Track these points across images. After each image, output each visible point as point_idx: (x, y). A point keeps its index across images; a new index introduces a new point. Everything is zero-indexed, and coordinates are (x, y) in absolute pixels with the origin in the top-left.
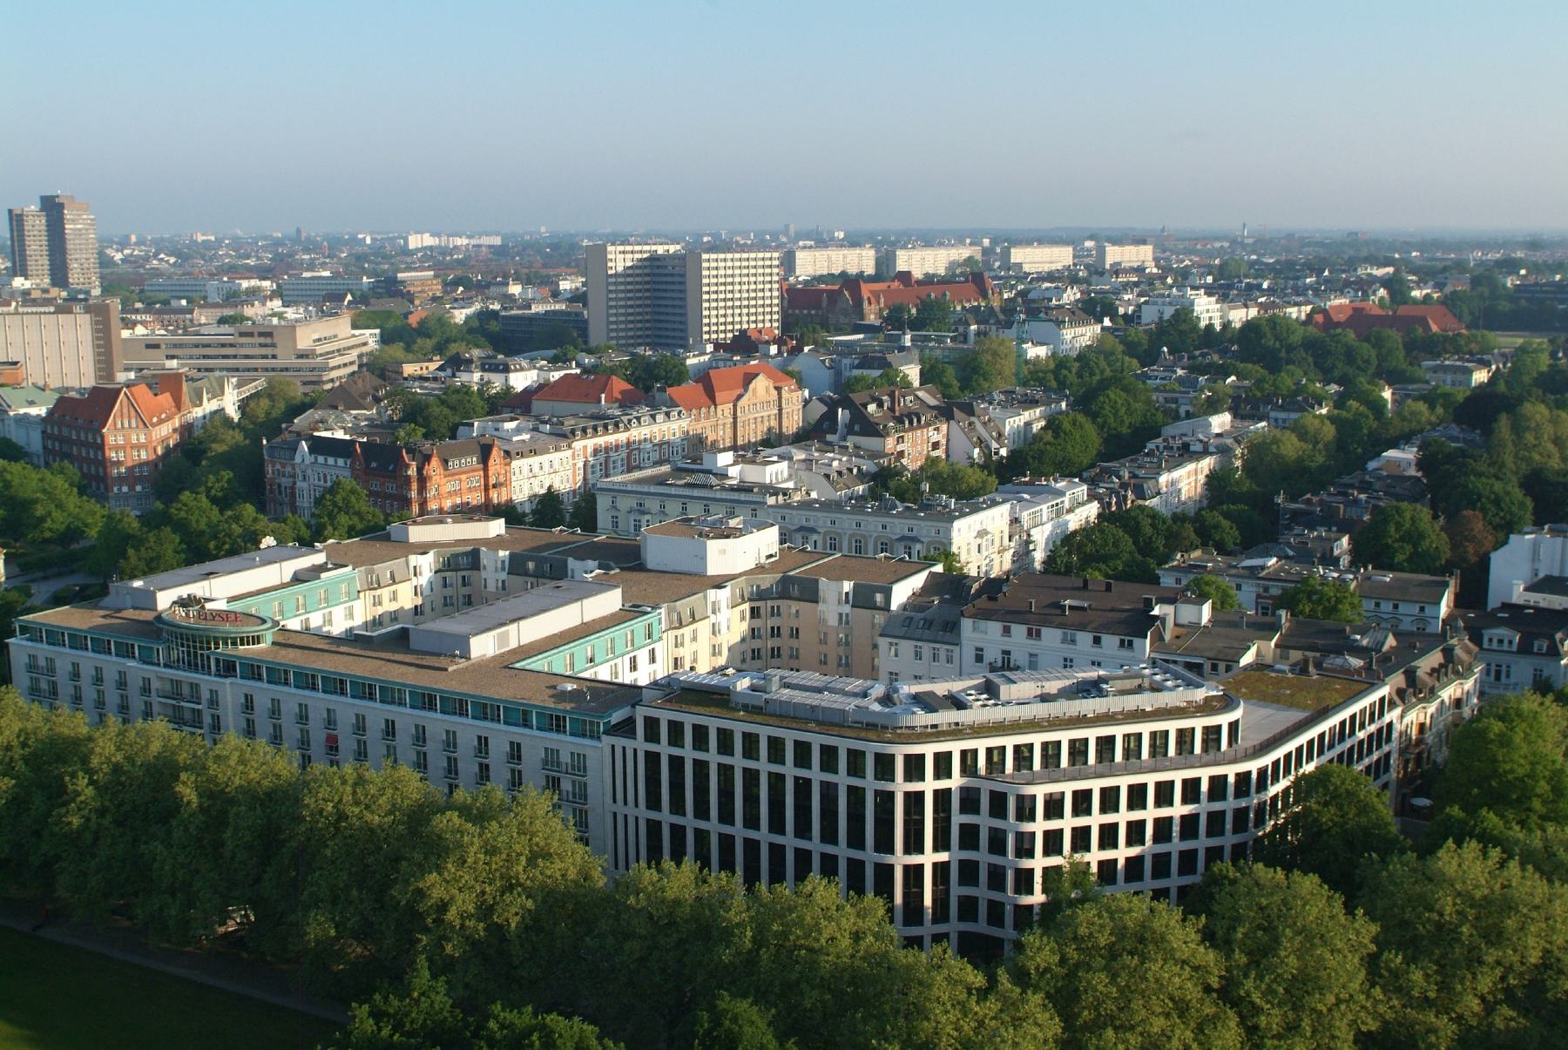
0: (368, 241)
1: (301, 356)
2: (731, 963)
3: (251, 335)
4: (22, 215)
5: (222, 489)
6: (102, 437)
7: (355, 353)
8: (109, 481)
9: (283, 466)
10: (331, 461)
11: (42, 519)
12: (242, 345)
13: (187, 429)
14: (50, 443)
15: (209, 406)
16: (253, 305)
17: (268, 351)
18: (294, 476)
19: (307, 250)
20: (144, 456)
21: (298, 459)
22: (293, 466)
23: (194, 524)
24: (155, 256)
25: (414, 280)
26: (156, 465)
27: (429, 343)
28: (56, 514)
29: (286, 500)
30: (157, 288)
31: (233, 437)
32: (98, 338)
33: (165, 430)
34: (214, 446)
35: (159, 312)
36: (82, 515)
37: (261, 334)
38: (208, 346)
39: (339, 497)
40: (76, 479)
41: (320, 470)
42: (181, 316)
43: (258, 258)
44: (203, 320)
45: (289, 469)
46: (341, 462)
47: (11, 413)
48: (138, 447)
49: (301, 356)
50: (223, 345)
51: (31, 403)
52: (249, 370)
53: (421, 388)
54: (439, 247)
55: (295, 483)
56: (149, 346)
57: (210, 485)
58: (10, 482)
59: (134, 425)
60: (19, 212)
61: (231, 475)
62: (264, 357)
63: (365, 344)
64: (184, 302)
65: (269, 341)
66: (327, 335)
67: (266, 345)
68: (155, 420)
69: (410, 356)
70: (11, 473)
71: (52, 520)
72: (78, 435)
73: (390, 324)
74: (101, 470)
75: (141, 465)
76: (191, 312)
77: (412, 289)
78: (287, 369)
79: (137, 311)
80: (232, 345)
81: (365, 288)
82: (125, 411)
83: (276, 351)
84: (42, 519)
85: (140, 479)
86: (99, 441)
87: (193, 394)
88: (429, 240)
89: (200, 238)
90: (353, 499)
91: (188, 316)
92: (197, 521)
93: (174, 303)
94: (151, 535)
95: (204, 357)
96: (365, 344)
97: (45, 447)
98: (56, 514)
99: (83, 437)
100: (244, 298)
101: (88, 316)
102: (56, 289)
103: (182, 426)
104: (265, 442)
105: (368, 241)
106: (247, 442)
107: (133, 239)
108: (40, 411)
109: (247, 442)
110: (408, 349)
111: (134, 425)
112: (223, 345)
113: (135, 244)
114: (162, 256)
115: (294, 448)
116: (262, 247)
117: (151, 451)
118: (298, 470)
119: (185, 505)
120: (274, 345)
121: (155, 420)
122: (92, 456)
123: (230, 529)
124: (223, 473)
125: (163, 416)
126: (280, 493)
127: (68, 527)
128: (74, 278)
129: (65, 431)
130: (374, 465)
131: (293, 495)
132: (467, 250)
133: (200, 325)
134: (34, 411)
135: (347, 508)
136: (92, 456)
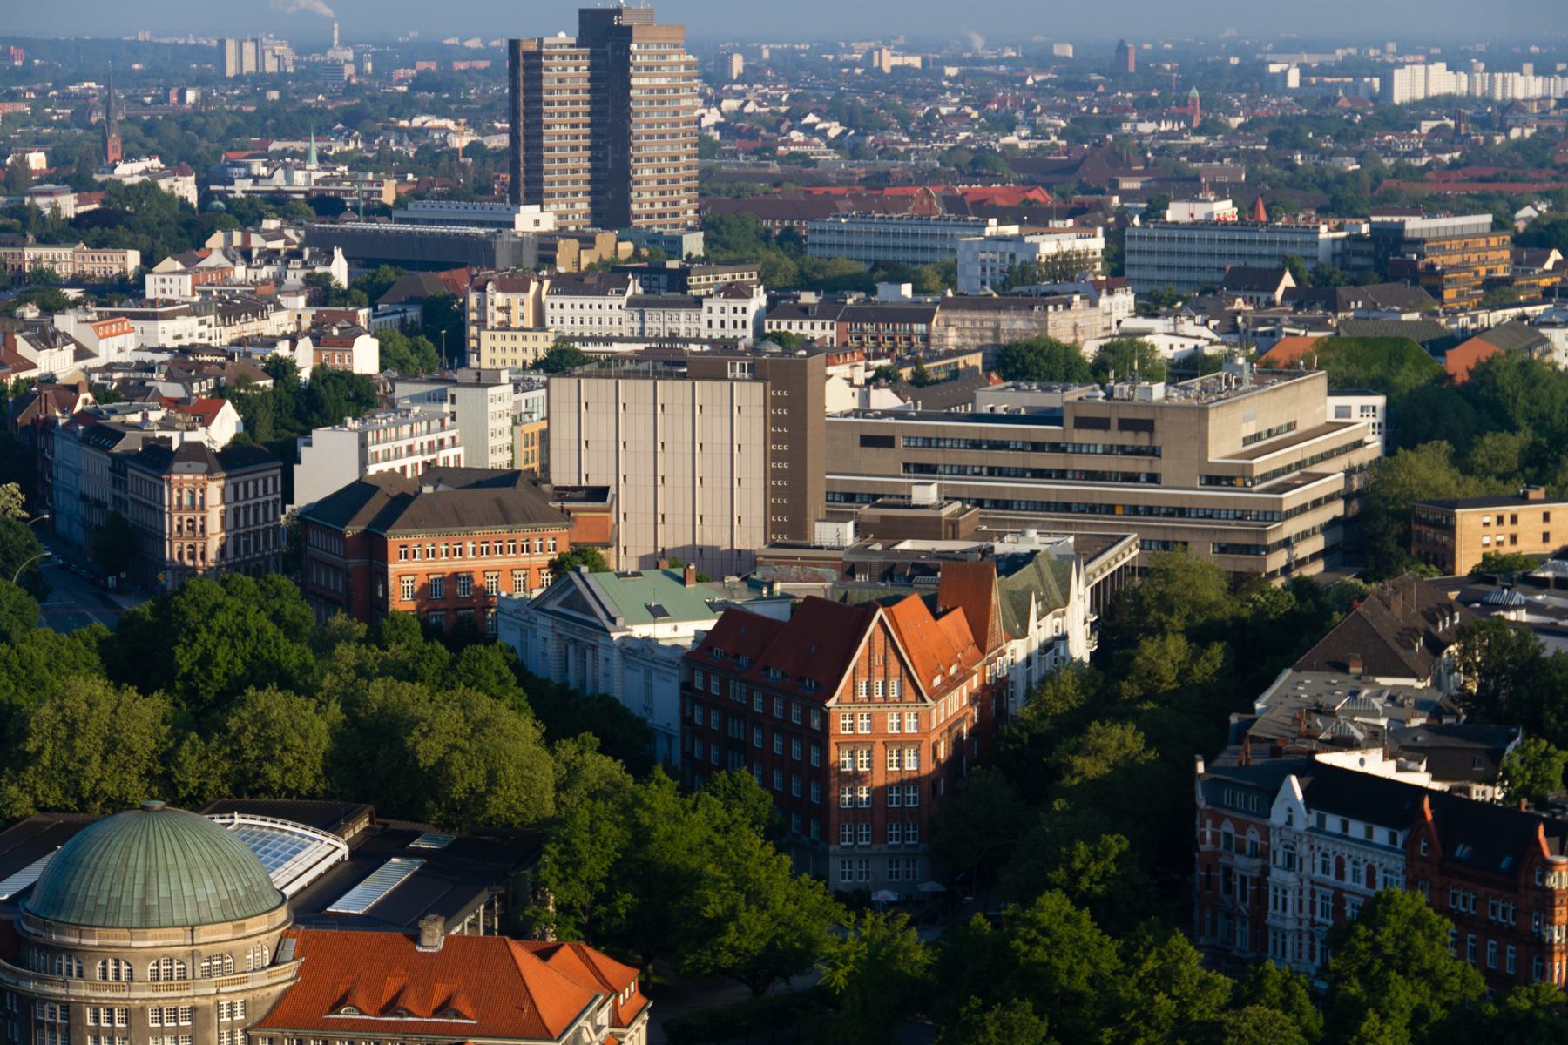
0: (1294, 80)
1: (1213, 480)
2: (1021, 999)
3: (1101, 424)
4: (539, 54)
5: (1105, 877)
6: (825, 717)
7: (1337, 467)
8: (834, 818)
9: (1241, 827)
10: (1357, 829)
11: (717, 926)
12: (1078, 449)
13: (994, 695)
14: (698, 713)
15: (1040, 630)
16: (1068, 305)
17: (1141, 465)
18: (1262, 853)
19: (1149, 109)
20: (910, 764)
21: (1277, 817)
22: (1265, 832)
23: (1063, 977)
24: (795, 117)
25: (1441, 241)
26: (935, 787)
27: (1509, 445)
28: (748, 916)
29: (1243, 908)
30: (836, 239)
31: (1122, 745)
32: (776, 438)
33: (955, 706)
34: (1078, 762)
35: (855, 315)
36: (800, 919)
37: (1125, 425)
38: (1002, 446)
39: (1387, 932)
40: (765, 810)
41: (1329, 846)
42: (903, 328)
43: (1037, 132)
44: (952, 339)
45: (1252, 836)
46: (1381, 835)
47: (616, 636)
48: (899, 744)
49: (1213, 480)
50: (1037, 447)
51: (658, 613)
52: (1093, 509)
53: (1532, 608)
54: (1469, 99)
55: (1266, 871)
56: (868, 441)
57: (1078, 865)
58: (649, 829)
59: (894, 692)
60: (533, 47)
61: (1125, 845)
62: (1131, 478)
63: (1359, 444)
64: (907, 290)
65: (1143, 440)
66: (1273, 425)
67: (1137, 452)
68: (937, 681)
69: (1471, 485)
70: (649, 808)
71: (741, 930)
72: (768, 704)
73: (1410, 378)
74: (814, 790)
75: (905, 784)
76: (926, 317)
77: (1439, 261)
78: (1182, 512)
79: (804, 312)
80: (1056, 447)
81: (1323, 253)
82: (878, 661)
83: (1159, 466)
84: (717, 926)
85: (901, 815)
86: (815, 724)
87: (1010, 612)
88: (1443, 81)
89: (889, 61)
90: (1420, 940)
91: (919, 328)
92: (1070, 972)
93: (884, 292)
94: (989, 1017)
95: (992, 471)
96: (1359, 444)
97: (686, 720)
98: (748, 916)
99: (778, 709)
100: (1046, 285)
101: (758, 388)
102: (611, 236)
103: (984, 687)
104: (1201, 768)
105: (1294, 80)
106: (1152, 755)
107: (738, 64)
108: (680, 632)
109: (1152, 755)
110: (1461, 461)
111: (894, 692)
112: (1037, 447)
113: (742, 79)
114: (811, 118)
115: (1271, 788)
116: (1039, 89)
117: (926, 754)
118: (1274, 841)
119: (1045, 932)
120: (1154, 452)
121: (937, 681)
122: (796, 756)
123: (1152, 1004)
124: (1110, 840)
125: (953, 670)
126: (1229, 888)
127: (771, 946)
128: (644, 201)
129: (737, 692)
130: (1462, 851)
131: (1261, 897)
132: (1544, 113)
133: (949, 354)
134: (662, 632)
135: (1405, 963)
136: (796, 756)
